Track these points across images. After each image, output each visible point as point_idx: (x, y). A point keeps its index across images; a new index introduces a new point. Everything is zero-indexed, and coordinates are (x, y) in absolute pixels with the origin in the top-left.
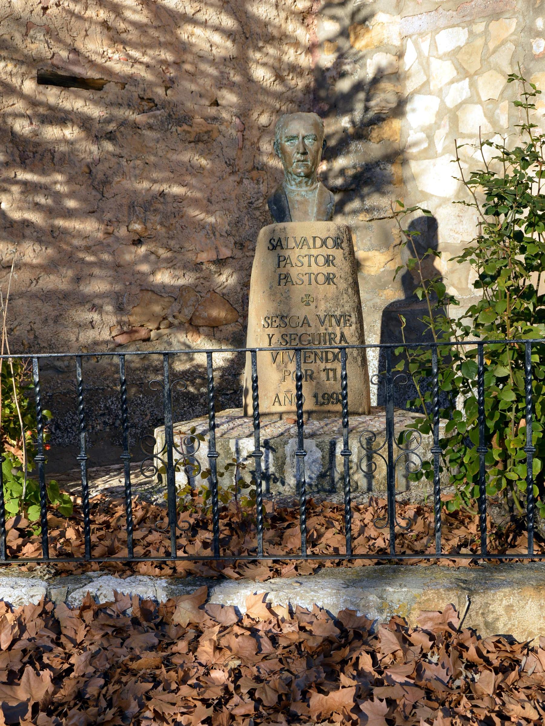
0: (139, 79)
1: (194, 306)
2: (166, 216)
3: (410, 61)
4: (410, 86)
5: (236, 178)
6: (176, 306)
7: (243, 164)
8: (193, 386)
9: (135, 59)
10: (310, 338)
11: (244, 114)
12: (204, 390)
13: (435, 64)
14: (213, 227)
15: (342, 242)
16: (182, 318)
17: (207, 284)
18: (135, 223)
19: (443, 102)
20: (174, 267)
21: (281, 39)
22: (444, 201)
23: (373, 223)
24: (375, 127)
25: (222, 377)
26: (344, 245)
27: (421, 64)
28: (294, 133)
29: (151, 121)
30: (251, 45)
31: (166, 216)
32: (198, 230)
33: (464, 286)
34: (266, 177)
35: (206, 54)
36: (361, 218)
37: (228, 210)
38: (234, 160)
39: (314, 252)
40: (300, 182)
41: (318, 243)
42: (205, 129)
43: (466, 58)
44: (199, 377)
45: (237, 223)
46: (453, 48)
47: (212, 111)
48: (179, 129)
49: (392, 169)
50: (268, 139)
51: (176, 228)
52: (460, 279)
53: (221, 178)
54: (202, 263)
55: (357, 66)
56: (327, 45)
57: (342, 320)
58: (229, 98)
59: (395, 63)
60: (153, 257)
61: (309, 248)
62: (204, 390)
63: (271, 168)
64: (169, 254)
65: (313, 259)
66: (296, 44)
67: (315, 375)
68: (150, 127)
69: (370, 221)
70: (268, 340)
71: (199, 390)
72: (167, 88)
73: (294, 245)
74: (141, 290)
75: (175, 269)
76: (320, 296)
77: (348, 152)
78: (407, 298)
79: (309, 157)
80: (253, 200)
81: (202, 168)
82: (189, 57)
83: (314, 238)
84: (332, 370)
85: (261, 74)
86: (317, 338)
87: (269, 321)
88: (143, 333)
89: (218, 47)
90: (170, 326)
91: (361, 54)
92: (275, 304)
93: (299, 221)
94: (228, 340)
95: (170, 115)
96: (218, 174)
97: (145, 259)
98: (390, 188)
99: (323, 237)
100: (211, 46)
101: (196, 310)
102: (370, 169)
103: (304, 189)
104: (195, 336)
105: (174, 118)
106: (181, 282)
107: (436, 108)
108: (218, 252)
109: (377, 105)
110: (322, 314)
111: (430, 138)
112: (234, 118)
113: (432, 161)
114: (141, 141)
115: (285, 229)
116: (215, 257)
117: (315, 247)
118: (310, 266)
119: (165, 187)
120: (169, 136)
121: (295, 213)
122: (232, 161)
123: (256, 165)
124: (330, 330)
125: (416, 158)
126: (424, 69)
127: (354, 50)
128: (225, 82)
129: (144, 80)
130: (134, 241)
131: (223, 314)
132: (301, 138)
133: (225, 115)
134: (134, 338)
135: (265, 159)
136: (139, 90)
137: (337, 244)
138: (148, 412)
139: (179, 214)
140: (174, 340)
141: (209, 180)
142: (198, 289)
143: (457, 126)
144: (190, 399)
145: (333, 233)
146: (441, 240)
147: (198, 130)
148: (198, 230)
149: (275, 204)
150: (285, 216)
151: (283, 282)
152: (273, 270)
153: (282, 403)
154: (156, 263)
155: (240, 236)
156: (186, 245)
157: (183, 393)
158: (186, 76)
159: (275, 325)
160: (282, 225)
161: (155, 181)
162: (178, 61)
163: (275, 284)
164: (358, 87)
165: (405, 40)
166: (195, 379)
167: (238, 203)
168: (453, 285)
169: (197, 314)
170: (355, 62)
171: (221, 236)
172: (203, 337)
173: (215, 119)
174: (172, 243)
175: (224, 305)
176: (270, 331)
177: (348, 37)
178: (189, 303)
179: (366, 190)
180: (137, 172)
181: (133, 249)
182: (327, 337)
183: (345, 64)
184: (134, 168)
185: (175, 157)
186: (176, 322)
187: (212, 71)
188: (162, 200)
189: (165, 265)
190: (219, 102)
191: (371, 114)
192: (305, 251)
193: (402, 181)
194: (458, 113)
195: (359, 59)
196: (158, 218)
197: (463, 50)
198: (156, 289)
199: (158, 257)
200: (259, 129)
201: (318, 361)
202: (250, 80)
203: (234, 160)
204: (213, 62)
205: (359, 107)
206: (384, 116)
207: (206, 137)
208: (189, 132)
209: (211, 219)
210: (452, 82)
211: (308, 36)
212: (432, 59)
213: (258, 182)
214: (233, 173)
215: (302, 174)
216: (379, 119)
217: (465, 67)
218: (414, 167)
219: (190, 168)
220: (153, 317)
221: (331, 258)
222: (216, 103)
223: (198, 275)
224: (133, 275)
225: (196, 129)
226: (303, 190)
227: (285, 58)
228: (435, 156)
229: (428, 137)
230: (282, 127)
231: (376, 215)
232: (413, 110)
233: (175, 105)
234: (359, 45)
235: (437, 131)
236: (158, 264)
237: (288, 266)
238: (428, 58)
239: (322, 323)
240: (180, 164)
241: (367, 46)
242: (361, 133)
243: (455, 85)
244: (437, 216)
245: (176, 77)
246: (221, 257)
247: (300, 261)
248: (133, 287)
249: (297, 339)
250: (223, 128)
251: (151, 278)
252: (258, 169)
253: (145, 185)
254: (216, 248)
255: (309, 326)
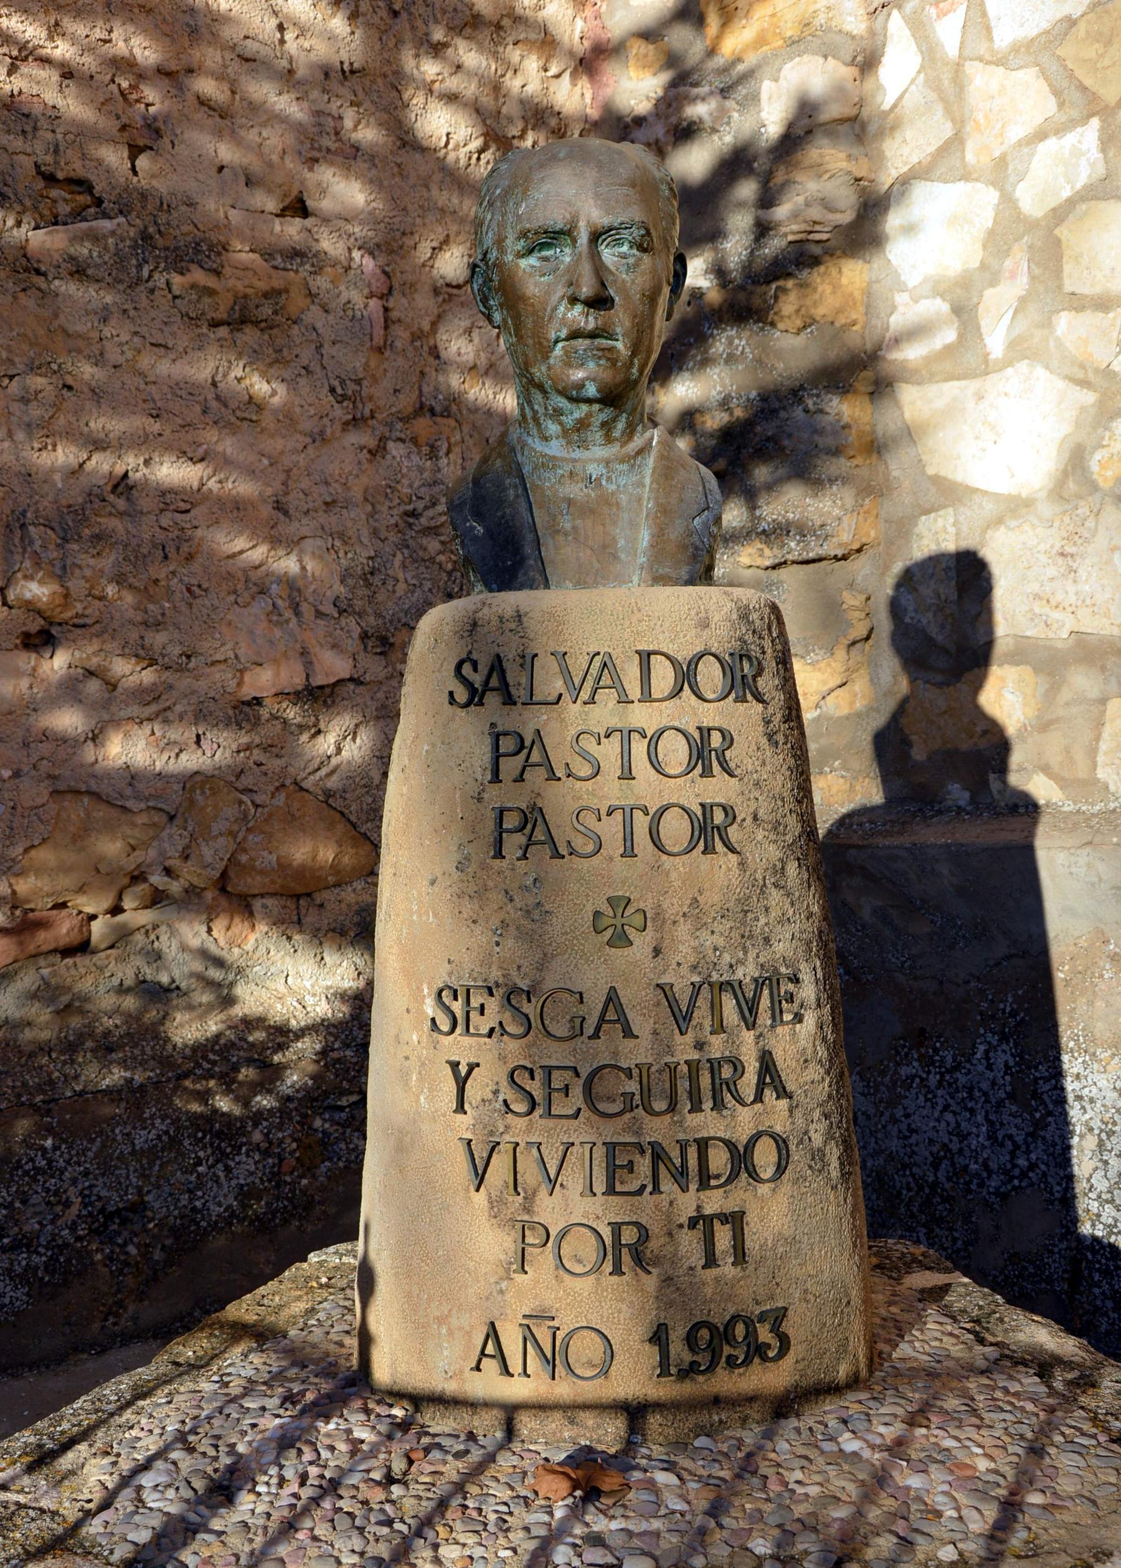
0: (37, 109)
1: (232, 834)
2: (136, 557)
3: (898, 75)
4: (900, 154)
5: (365, 438)
6: (173, 840)
7: (386, 394)
8: (228, 1091)
9: (23, 47)
10: (633, 1086)
11: (391, 244)
12: (264, 1101)
13: (983, 81)
14: (293, 588)
15: (760, 672)
16: (190, 874)
17: (274, 764)
18: (29, 578)
19: (1008, 200)
20: (163, 716)
21: (499, 27)
22: (1015, 507)
23: (783, 573)
24: (790, 284)
25: (323, 1053)
26: (767, 683)
27: (934, 85)
28: (556, 218)
29: (83, 250)
30: (408, 36)
31: (136, 557)
32: (245, 597)
33: (1082, 773)
34: (457, 437)
35: (265, 51)
36: (745, 560)
37: (341, 535)
38: (358, 382)
39: (643, 716)
40: (582, 425)
41: (663, 676)
42: (262, 285)
43: (1090, 52)
44: (250, 1061)
45: (369, 575)
46: (1045, 25)
47: (292, 230)
48: (177, 280)
49: (844, 409)
50: (466, 323)
51: (169, 593)
52: (1067, 750)
53: (320, 438)
54: (258, 701)
55: (730, 104)
56: (638, 48)
57: (765, 1002)
58: (346, 192)
59: (850, 85)
60: (93, 686)
61: (624, 700)
62: (264, 1101)
63: (475, 409)
64: (148, 676)
65: (639, 748)
66: (546, 42)
67: (654, 1244)
68: (79, 271)
69: (774, 567)
70: (450, 1087)
71: (246, 1104)
72: (135, 151)
73: (559, 685)
74: (56, 793)
75: (166, 721)
76: (674, 905)
77: (706, 362)
78: (892, 800)
79: (621, 319)
80: (420, 505)
81: (252, 402)
82: (212, 57)
83: (645, 658)
84: (724, 1218)
85: (443, 126)
86: (661, 1084)
87: (457, 1007)
88: (64, 928)
89: (302, 32)
90: (157, 898)
91: (741, 68)
92: (481, 937)
93: (581, 583)
94: (343, 933)
95: (145, 236)
96: (307, 425)
97: (69, 690)
98: (841, 465)
99: (684, 655)
100: (281, 28)
101: (241, 848)
102: (774, 412)
103: (599, 451)
104: (240, 927)
105: (161, 247)
106: (190, 761)
107: (986, 219)
108: (308, 665)
109: (795, 215)
110: (681, 982)
111: (964, 313)
112: (356, 254)
113: (972, 385)
114: (46, 313)
115: (519, 617)
116: (299, 681)
117: (647, 697)
118: (627, 775)
119: (130, 462)
120: (144, 302)
121: (560, 552)
122: (351, 387)
123: (429, 401)
124: (717, 1047)
125: (915, 376)
126: (943, 99)
127: (719, 61)
128: (327, 142)
129: (54, 116)
130: (27, 635)
131: (327, 854)
132: (583, 239)
133: (329, 244)
134: (32, 948)
135: (455, 381)
136: (39, 147)
137: (741, 683)
138: (72, 1193)
139: (178, 547)
140: (167, 945)
141: (279, 444)
142: (247, 781)
143: (1058, 273)
144: (219, 1135)
145: (721, 637)
146: (1002, 628)
147: (239, 286)
148: (245, 597)
149: (479, 516)
150: (520, 561)
151: (513, 843)
152: (473, 789)
153: (515, 1365)
154: (106, 705)
155: (378, 615)
156: (205, 646)
157: (194, 1118)
158: (200, 115)
159: (482, 1024)
160: (509, 601)
161: (98, 445)
162: (173, 66)
163: (481, 850)
164: (735, 163)
165: (881, 17)
166: (236, 1069)
167: (371, 515)
168: (1046, 769)
169: (244, 858)
170: (725, 92)
171: (319, 614)
172: (262, 927)
173: (297, 254)
174: (158, 639)
175: (331, 827)
176: (461, 1047)
177: (700, 21)
178: (216, 828)
179: (762, 473)
180: (35, 412)
181: (25, 660)
182: (705, 1080)
183: (694, 100)
184: (25, 400)
185: (165, 368)
186: (175, 887)
187: (285, 104)
188: (121, 504)
189: (134, 710)
190: (310, 203)
191: (774, 245)
192: (605, 712)
193: (875, 447)
194: (1062, 232)
195: (734, 85)
196: (108, 562)
197: (1082, 27)
198: (104, 789)
199: (112, 686)
200: (436, 291)
201: (668, 1185)
202: (406, 140)
203: (358, 382)
204: (288, 77)
205: (739, 225)
206: (817, 250)
207: (266, 311)
208: (211, 292)
209: (289, 564)
210: (1041, 135)
211: (579, 24)
212: (970, 68)
213: (433, 454)
214: (355, 422)
215: (591, 390)
216: (803, 258)
217: (1088, 82)
218: (914, 401)
219: (214, 404)
220: (99, 874)
221: (716, 740)
222: (299, 208)
223: (245, 739)
224: (26, 745)
225: (233, 282)
226: (596, 455)
227: (513, 84)
228: (986, 368)
229: (958, 310)
230: (507, 193)
231: (794, 548)
232: (910, 229)
233: (164, 206)
234: (731, 44)
235: (989, 293)
236: (111, 706)
237: (535, 777)
238: (958, 67)
239: (682, 1019)
240: (185, 390)
241: (760, 40)
242: (747, 300)
243: (1052, 143)
244: (988, 554)
245: (167, 118)
246: (319, 680)
247: (585, 756)
248: (25, 783)
249: (577, 1091)
250: (321, 283)
251: (89, 753)
252: (432, 411)
253: (64, 455)
254: (304, 653)
255: (628, 1033)
